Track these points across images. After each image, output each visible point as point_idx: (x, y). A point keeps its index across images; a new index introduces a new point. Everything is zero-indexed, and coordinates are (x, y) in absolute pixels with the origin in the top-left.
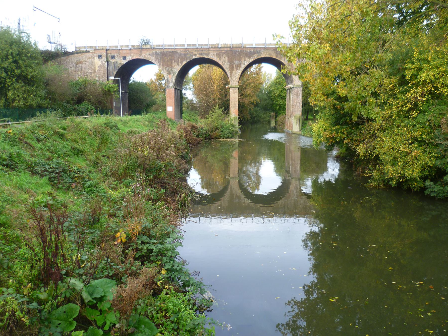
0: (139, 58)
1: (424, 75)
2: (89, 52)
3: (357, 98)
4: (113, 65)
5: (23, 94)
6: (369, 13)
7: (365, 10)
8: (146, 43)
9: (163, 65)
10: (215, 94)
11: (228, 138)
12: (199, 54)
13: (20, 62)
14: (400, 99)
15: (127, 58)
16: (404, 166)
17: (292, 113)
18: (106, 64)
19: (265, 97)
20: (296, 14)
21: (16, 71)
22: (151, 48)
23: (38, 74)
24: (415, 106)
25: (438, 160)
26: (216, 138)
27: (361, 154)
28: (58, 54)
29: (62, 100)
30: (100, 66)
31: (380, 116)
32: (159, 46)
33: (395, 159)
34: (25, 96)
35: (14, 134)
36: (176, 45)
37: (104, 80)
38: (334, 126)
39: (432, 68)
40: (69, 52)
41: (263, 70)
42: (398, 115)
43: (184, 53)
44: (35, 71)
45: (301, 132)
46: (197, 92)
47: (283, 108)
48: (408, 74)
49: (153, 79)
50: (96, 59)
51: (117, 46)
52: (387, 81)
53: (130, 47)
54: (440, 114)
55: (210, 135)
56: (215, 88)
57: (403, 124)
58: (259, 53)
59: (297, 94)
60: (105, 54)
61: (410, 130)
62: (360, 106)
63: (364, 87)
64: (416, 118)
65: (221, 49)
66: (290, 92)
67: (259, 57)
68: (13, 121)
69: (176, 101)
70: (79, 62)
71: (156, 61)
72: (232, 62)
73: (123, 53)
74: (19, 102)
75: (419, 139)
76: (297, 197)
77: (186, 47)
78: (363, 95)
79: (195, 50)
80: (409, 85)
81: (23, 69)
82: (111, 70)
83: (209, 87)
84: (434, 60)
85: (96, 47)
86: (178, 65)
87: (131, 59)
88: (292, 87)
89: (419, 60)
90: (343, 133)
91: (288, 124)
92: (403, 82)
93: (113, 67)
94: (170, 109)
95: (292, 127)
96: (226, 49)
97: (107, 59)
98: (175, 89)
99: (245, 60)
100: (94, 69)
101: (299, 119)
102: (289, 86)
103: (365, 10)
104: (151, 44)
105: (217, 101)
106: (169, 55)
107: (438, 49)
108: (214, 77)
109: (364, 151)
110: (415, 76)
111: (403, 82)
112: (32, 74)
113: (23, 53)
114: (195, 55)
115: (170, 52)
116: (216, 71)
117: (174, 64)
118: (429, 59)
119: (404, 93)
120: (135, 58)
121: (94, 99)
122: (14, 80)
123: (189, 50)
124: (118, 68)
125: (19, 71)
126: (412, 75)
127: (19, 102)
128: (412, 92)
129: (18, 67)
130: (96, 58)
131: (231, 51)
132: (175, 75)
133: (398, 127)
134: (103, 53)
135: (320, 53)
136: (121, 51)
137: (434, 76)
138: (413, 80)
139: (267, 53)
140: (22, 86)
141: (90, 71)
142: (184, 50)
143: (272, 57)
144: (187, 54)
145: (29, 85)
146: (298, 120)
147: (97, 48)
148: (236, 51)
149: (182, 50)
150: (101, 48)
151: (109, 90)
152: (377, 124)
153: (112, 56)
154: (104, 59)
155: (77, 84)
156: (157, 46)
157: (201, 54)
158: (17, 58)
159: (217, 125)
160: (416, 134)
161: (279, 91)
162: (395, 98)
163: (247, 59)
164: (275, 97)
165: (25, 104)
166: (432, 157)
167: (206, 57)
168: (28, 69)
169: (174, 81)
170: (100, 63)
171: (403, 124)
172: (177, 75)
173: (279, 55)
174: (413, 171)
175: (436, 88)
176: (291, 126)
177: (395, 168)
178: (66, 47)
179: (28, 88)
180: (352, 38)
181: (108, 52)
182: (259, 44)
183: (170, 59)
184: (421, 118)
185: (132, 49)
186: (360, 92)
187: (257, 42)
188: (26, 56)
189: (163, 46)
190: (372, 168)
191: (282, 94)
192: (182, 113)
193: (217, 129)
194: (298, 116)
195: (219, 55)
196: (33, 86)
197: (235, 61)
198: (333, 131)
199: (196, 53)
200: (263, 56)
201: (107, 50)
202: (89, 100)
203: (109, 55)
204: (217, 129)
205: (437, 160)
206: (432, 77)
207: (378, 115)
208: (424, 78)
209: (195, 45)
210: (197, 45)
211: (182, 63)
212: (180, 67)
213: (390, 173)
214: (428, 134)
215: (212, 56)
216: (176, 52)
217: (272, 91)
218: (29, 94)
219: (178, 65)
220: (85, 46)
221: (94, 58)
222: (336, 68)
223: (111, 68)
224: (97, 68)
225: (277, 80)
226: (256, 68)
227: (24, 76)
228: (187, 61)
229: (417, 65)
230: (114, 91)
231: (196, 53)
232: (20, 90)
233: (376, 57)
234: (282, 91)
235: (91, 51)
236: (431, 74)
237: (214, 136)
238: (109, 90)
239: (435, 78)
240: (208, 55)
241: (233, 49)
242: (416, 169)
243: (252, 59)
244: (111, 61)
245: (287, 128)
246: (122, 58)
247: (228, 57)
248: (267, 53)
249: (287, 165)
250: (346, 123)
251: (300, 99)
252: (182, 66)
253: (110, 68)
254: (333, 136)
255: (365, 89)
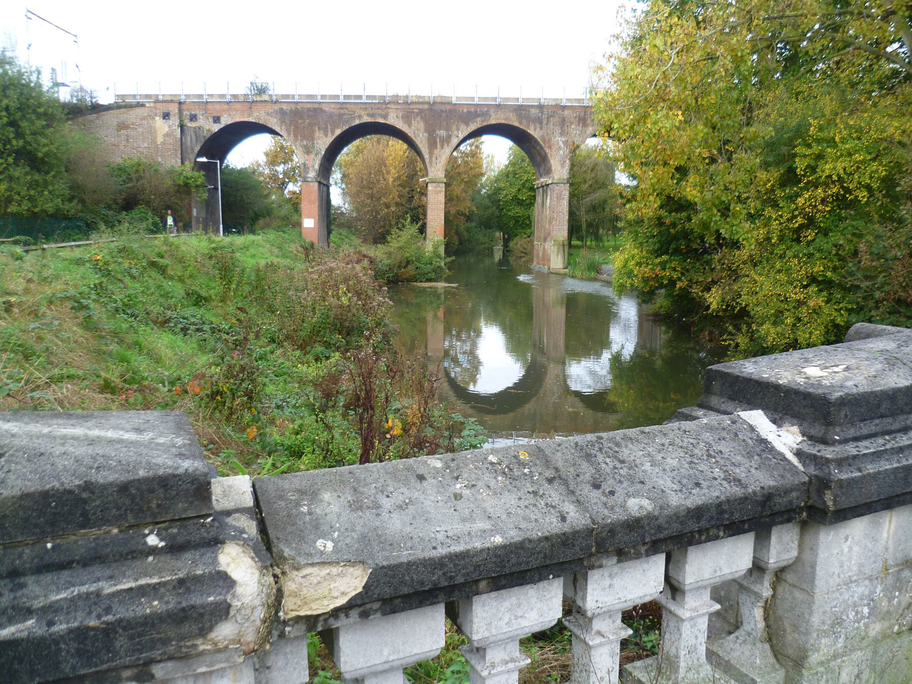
0: (246, 120)
1: (827, 166)
2: (143, 105)
3: (713, 204)
4: (193, 134)
5: (28, 189)
6: (745, 58)
7: (739, 54)
8: (262, 91)
9: (296, 136)
10: (390, 194)
11: (429, 280)
12: (368, 115)
13: (24, 124)
14: (785, 209)
15: (222, 119)
16: (794, 325)
17: (549, 234)
18: (179, 130)
19: (487, 202)
20: (608, 53)
21: (14, 142)
22: (272, 101)
23: (57, 149)
24: (811, 222)
25: (853, 315)
26: (409, 281)
27: (714, 306)
28: (79, 108)
29: (97, 203)
30: (167, 135)
31: (752, 237)
32: (287, 96)
33: (780, 313)
34: (32, 192)
35: (105, 263)
36: (323, 97)
37: (172, 162)
38: (656, 257)
39: (842, 155)
40: (102, 106)
41: (484, 147)
42: (781, 239)
43: (337, 112)
44: (52, 144)
45: (567, 270)
46: (354, 190)
47: (524, 224)
48: (800, 165)
49: (260, 162)
50: (159, 121)
51: (201, 96)
52: (762, 175)
53: (228, 98)
54: (854, 234)
55: (396, 275)
56: (390, 182)
57: (789, 253)
58: (486, 115)
59: (560, 197)
60: (177, 111)
61: (804, 262)
62: (718, 218)
63: (725, 185)
64: (814, 240)
65: (411, 107)
66: (545, 193)
67: (485, 124)
68: (63, 241)
69: (320, 207)
70: (122, 126)
71: (281, 127)
72: (434, 131)
73: (215, 110)
74: (19, 205)
75: (820, 279)
76: (560, 398)
77: (342, 100)
78: (723, 198)
79: (360, 106)
80: (802, 185)
81: (29, 138)
82: (189, 143)
83: (378, 181)
84: (844, 141)
85: (157, 96)
86: (326, 135)
87: (230, 122)
88: (550, 182)
89: (818, 141)
90: (674, 270)
91: (541, 254)
92: (790, 178)
93: (194, 138)
94: (309, 223)
95: (549, 260)
96: (420, 107)
97: (181, 121)
98: (320, 183)
99: (458, 129)
100: (154, 141)
101: (563, 245)
102: (542, 180)
103: (739, 54)
104: (271, 92)
105: (393, 209)
106: (309, 117)
107: (851, 123)
108: (389, 161)
109: (720, 300)
110: (813, 169)
111: (790, 178)
112: (47, 149)
113: (28, 106)
114: (360, 117)
115: (309, 110)
116: (397, 147)
117: (318, 134)
118: (837, 139)
119: (792, 198)
120: (238, 120)
121: (157, 201)
122: (11, 160)
123: (348, 106)
124: (203, 141)
125: (21, 142)
126: (807, 167)
127: (19, 205)
128: (807, 196)
129: (19, 135)
130: (157, 118)
131: (431, 110)
132: (320, 157)
133: (782, 257)
134: (174, 109)
135: (667, 125)
136: (209, 106)
137: (845, 169)
138: (809, 177)
139: (502, 116)
140: (26, 174)
141: (146, 145)
142: (338, 106)
143: (510, 123)
144: (344, 114)
145: (39, 171)
146: (561, 248)
147: (161, 98)
148: (442, 111)
149: (333, 106)
150: (169, 98)
151: (186, 185)
152: (744, 254)
153: (191, 115)
154: (174, 121)
155: (120, 169)
156: (284, 96)
157: (372, 116)
158: (19, 115)
159: (408, 255)
160: (815, 270)
161: (514, 190)
162: (775, 205)
163: (463, 126)
164: (506, 202)
165: (32, 209)
166: (841, 309)
167: (381, 121)
168: (40, 138)
169: (317, 167)
170: (167, 129)
171: (789, 253)
172: (325, 155)
173: (524, 121)
174: (811, 333)
175: (848, 191)
176: (546, 259)
177: (779, 329)
178: (95, 94)
179: (37, 176)
180: (708, 101)
181: (184, 107)
182: (486, 99)
183: (309, 123)
184: (821, 242)
185: (235, 101)
186: (718, 193)
187: (504, 94)
188: (34, 111)
189: (296, 97)
190: (734, 331)
191: (520, 197)
192: (329, 232)
193: (408, 263)
194: (562, 239)
195: (407, 117)
196: (47, 173)
197: (440, 129)
198: (657, 265)
199: (362, 113)
200: (493, 121)
201: (180, 103)
202: (148, 203)
203: (185, 113)
204: (408, 263)
205: (849, 314)
206: (842, 172)
207: (750, 236)
208: (827, 172)
209: (360, 97)
210: (364, 98)
211: (333, 133)
212: (330, 139)
213: (770, 339)
214: (835, 269)
215: (394, 120)
216: (321, 109)
217: (500, 189)
218: (40, 189)
219: (326, 135)
220: (135, 93)
221: (153, 119)
222: (683, 152)
223: (189, 139)
224: (160, 140)
225: (511, 169)
226: (471, 145)
227: (29, 153)
228: (344, 128)
229: (816, 149)
230: (197, 186)
231: (362, 113)
232: (22, 180)
233: (746, 132)
234: (519, 190)
235: (148, 105)
236: (840, 166)
237: (404, 277)
238: (186, 185)
239: (845, 173)
240: (385, 117)
241: (434, 108)
242: (816, 329)
243: (473, 127)
244: (189, 125)
245: (538, 263)
246: (211, 120)
247: (426, 122)
248: (502, 116)
249: (537, 337)
250: (677, 252)
251: (564, 206)
252: (334, 137)
253: (186, 139)
254: (657, 275)
255: (726, 189)
